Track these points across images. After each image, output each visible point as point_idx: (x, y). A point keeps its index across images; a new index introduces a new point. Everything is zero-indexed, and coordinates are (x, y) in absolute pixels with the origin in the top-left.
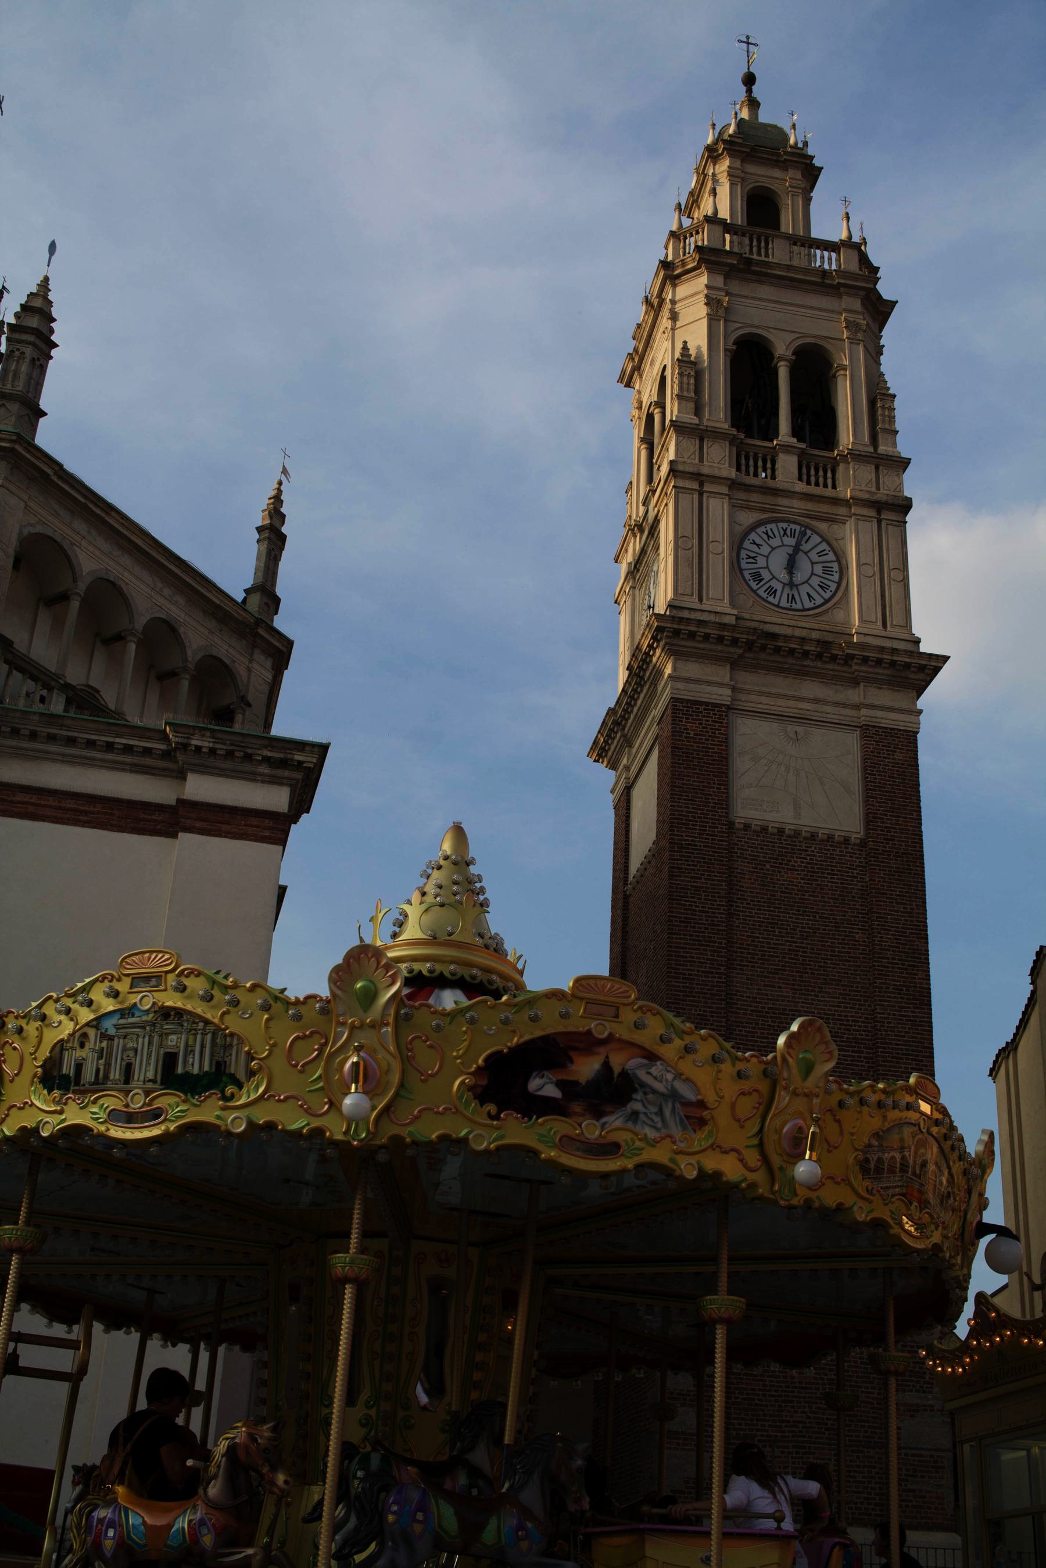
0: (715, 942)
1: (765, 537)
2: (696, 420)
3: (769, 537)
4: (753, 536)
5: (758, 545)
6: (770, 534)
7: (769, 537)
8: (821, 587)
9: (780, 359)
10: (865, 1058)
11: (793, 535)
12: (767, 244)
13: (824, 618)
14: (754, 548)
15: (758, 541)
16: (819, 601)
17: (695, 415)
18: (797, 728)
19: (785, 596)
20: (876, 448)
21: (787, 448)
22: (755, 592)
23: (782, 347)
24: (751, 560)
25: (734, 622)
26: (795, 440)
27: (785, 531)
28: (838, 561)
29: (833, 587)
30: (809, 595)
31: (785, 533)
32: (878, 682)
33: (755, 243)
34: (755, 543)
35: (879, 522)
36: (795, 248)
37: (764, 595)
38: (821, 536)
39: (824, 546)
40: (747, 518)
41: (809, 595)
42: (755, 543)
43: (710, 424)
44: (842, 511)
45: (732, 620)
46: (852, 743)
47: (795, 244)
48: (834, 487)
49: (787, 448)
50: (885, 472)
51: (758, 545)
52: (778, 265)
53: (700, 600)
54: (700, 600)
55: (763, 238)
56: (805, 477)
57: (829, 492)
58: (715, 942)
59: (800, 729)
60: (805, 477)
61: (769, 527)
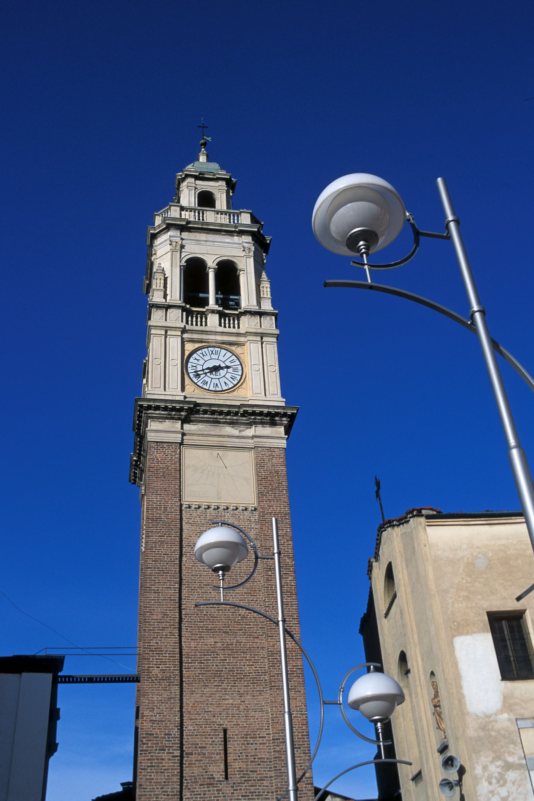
0: (172, 571)
1: (202, 356)
2: (164, 300)
3: (203, 355)
4: (195, 356)
5: (197, 360)
6: (204, 354)
7: (203, 355)
8: (232, 378)
9: (209, 268)
10: (260, 628)
11: (216, 354)
12: (203, 214)
13: (235, 393)
14: (196, 361)
15: (198, 358)
16: (231, 385)
17: (164, 298)
18: (218, 452)
19: (212, 384)
20: (260, 307)
21: (213, 312)
22: (196, 384)
23: (211, 262)
24: (194, 368)
25: (183, 399)
26: (217, 306)
27: (212, 352)
28: (241, 364)
29: (239, 378)
30: (225, 383)
31: (212, 353)
32: (262, 423)
33: (232, 217)
34: (196, 359)
35: (262, 343)
36: (219, 216)
37: (201, 385)
38: (231, 352)
39: (234, 357)
40: (190, 347)
41: (225, 383)
42: (196, 359)
43: (170, 302)
44: (242, 339)
45: (182, 398)
46: (249, 458)
47: (218, 214)
48: (239, 327)
49: (213, 312)
50: (155, 310)
51: (197, 360)
52: (212, 224)
53: (165, 390)
54: (165, 390)
55: (201, 212)
56: (223, 324)
57: (203, 328)
58: (172, 571)
59: (221, 453)
60: (223, 324)
61: (203, 350)
